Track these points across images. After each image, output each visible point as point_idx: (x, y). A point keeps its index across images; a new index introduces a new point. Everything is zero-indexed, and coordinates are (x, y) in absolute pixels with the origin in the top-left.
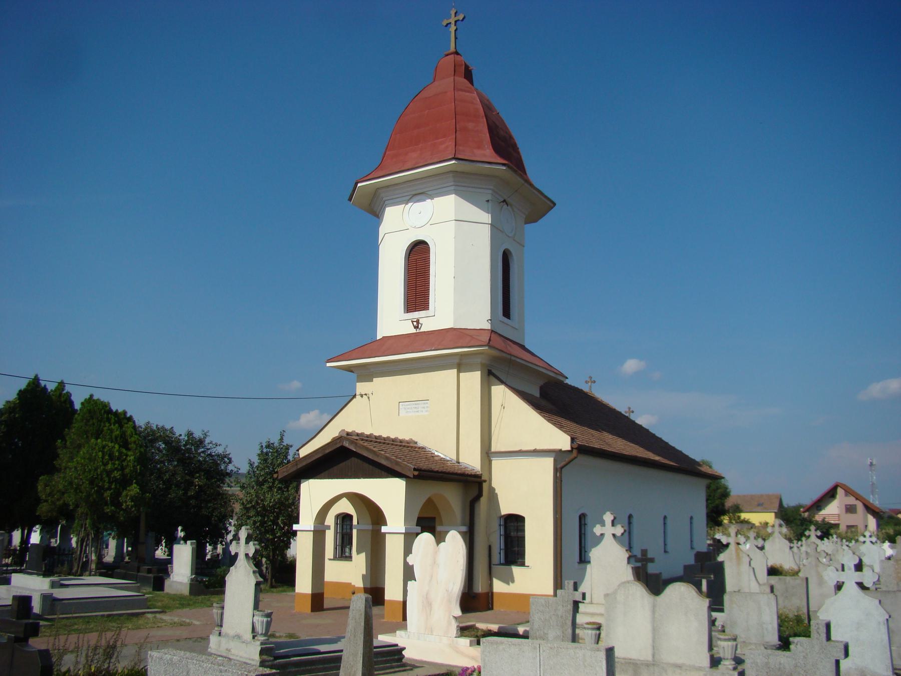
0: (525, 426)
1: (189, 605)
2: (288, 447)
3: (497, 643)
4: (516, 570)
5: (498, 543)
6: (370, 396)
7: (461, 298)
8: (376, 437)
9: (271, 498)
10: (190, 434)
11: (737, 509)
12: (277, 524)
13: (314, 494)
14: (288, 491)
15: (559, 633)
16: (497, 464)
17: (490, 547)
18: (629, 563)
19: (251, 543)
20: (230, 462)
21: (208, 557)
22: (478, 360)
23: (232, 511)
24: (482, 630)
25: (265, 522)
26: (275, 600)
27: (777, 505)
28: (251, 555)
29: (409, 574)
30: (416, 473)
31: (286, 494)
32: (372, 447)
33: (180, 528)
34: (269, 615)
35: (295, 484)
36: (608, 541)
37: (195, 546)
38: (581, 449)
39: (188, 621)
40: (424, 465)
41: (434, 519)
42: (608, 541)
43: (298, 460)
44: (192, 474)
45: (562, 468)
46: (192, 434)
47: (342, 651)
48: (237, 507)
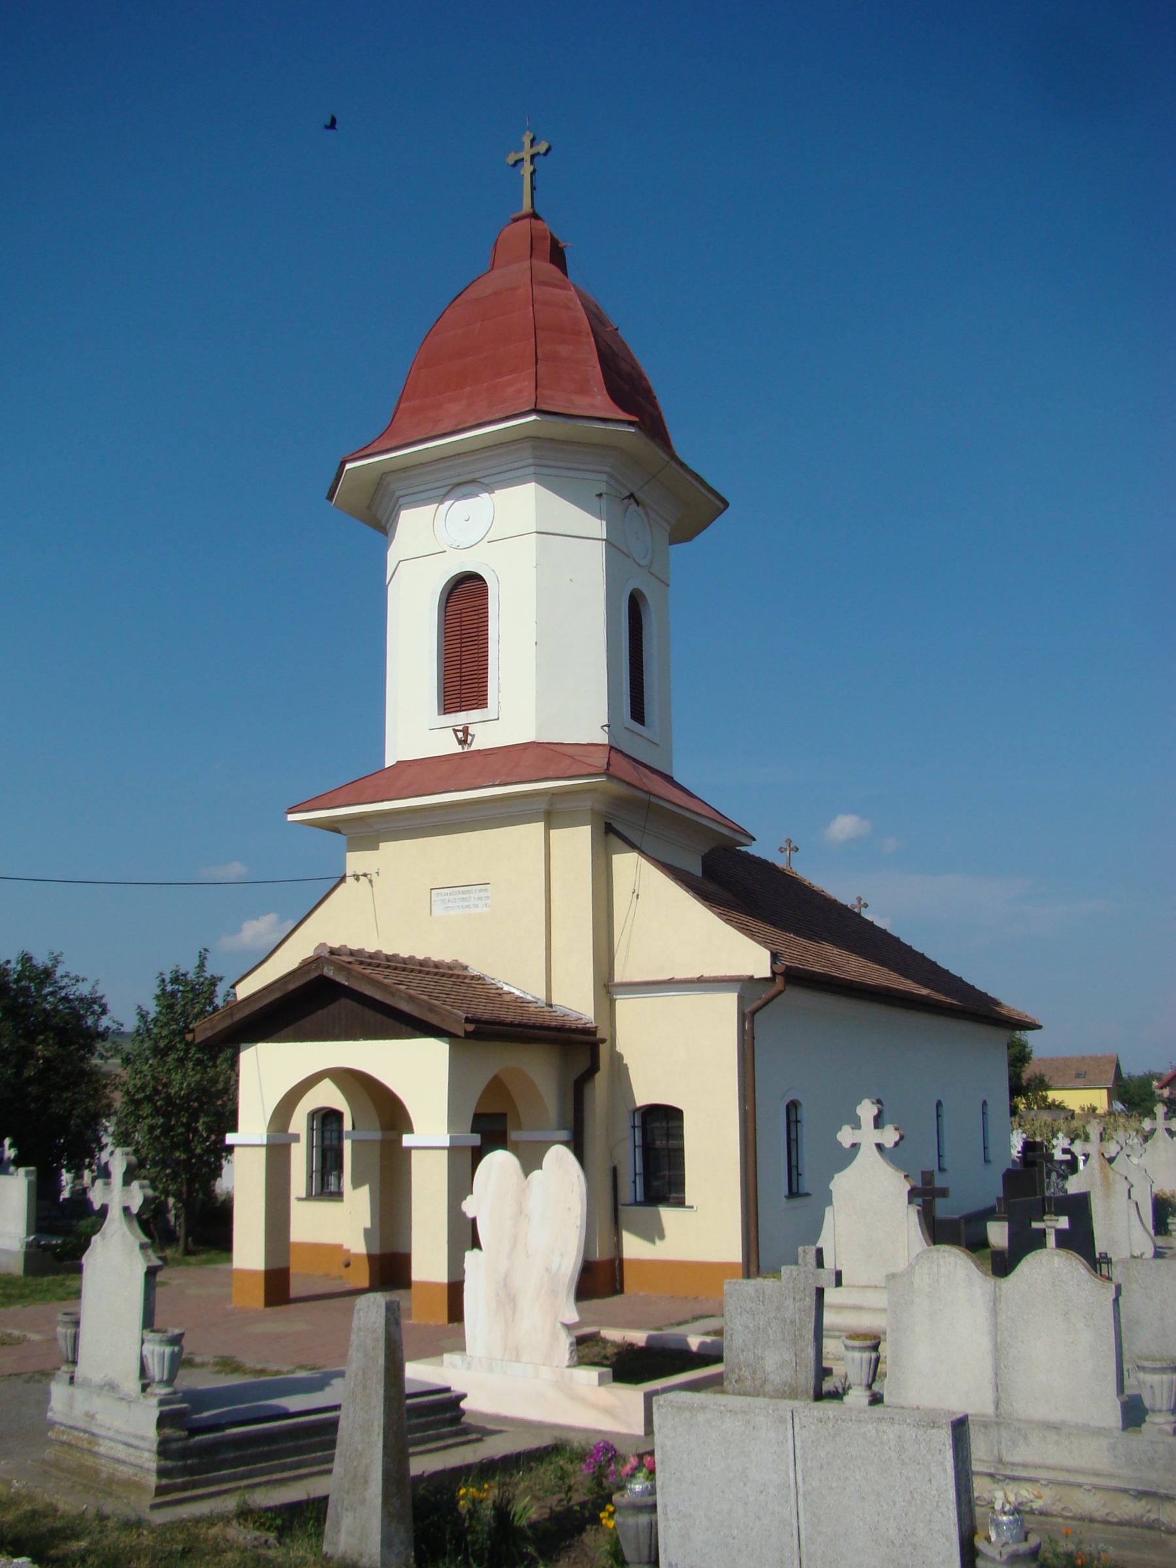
0: (679, 932)
1: (22, 1297)
2: (214, 982)
3: (691, 1408)
4: (667, 1214)
5: (630, 1162)
6: (374, 877)
7: (550, 683)
8: (388, 958)
9: (181, 1082)
10: (26, 959)
11: (1042, 1084)
12: (196, 1130)
13: (268, 1072)
14: (215, 1066)
15: (788, 1356)
16: (625, 1006)
17: (615, 1170)
18: (910, 1202)
19: (135, 1184)
20: (104, 1012)
21: (65, 1194)
22: (588, 803)
23: (110, 1106)
24: (614, 1343)
25: (172, 1128)
26: (188, 1280)
27: (1111, 1075)
28: (135, 1210)
29: (465, 1235)
30: (471, 1027)
31: (211, 1072)
32: (380, 978)
33: (7, 1142)
34: (176, 1340)
35: (228, 1052)
36: (868, 1157)
37: (33, 1178)
38: (791, 977)
39: (16, 1333)
40: (484, 1011)
41: (502, 1116)
42: (868, 1157)
43: (234, 1006)
44: (31, 1036)
45: (754, 1013)
46: (30, 959)
47: (337, 1408)
48: (118, 1099)
